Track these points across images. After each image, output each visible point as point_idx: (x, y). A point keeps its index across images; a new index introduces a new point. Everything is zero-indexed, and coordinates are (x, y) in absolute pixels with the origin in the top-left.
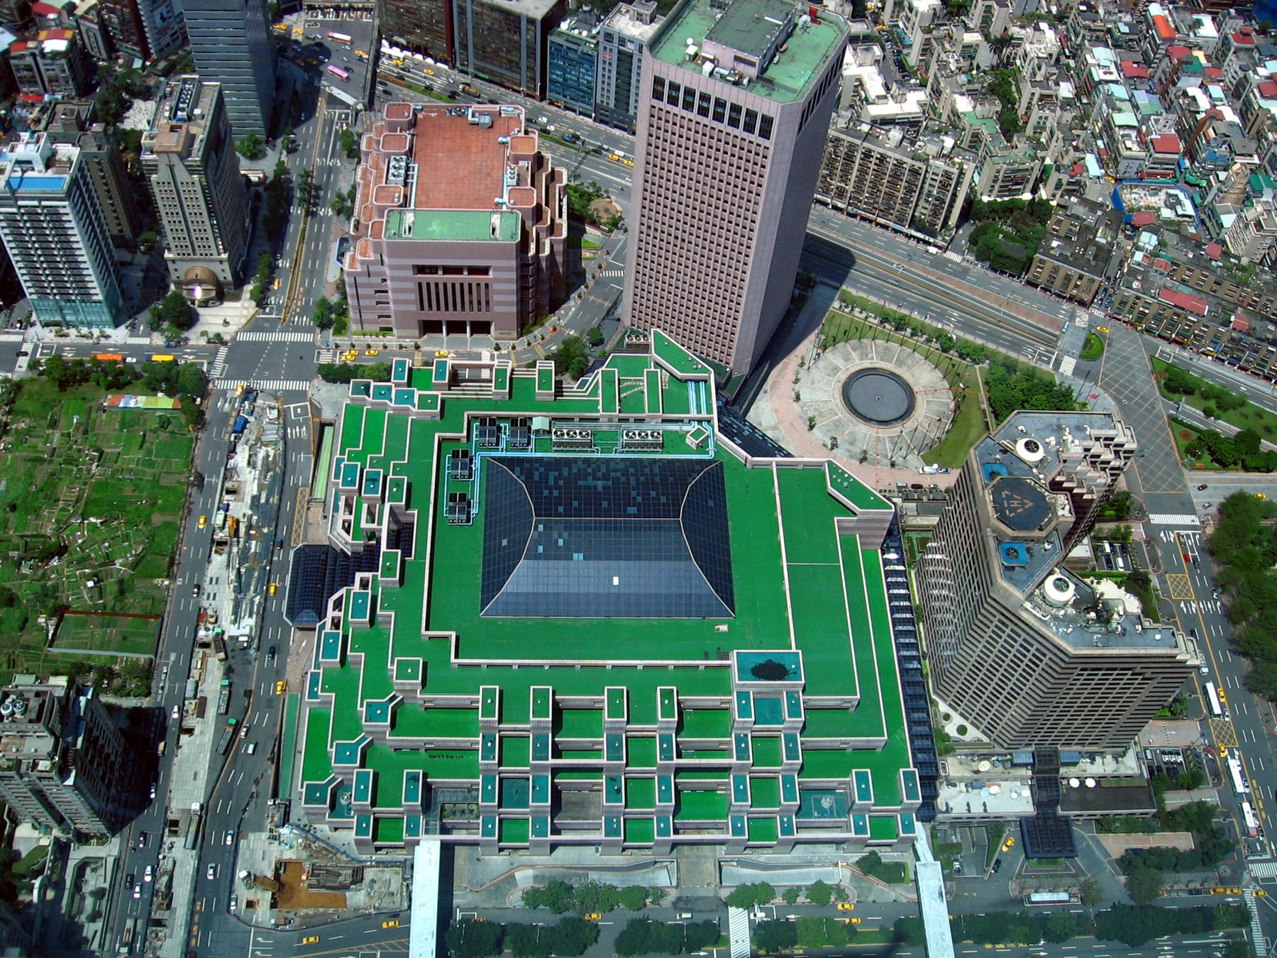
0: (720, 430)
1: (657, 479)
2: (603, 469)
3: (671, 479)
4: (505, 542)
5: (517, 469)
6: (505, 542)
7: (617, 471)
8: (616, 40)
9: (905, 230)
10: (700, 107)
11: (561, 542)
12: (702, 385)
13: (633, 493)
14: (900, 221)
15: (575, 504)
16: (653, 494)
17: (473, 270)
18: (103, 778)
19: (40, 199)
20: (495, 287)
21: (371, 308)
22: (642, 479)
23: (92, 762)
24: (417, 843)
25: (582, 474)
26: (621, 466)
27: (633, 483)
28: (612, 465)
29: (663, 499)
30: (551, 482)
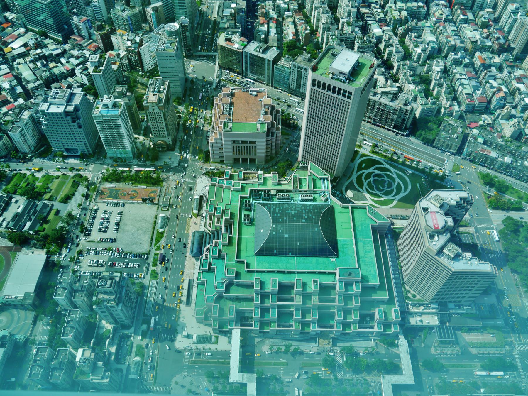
0: (332, 195)
1: (312, 211)
2: (294, 207)
3: (316, 211)
4: (262, 231)
5: (266, 207)
6: (262, 231)
7: (298, 208)
8: (297, 67)
9: (392, 129)
10: (348, 96)
11: (280, 231)
12: (326, 181)
13: (304, 215)
14: (390, 126)
15: (285, 218)
16: (310, 215)
17: (251, 142)
18: (130, 307)
19: (110, 117)
20: (258, 147)
21: (217, 154)
22: (307, 211)
23: (127, 301)
24: (233, 329)
25: (287, 209)
26: (300, 206)
27: (304, 211)
28: (297, 206)
29: (314, 217)
30: (277, 211)
